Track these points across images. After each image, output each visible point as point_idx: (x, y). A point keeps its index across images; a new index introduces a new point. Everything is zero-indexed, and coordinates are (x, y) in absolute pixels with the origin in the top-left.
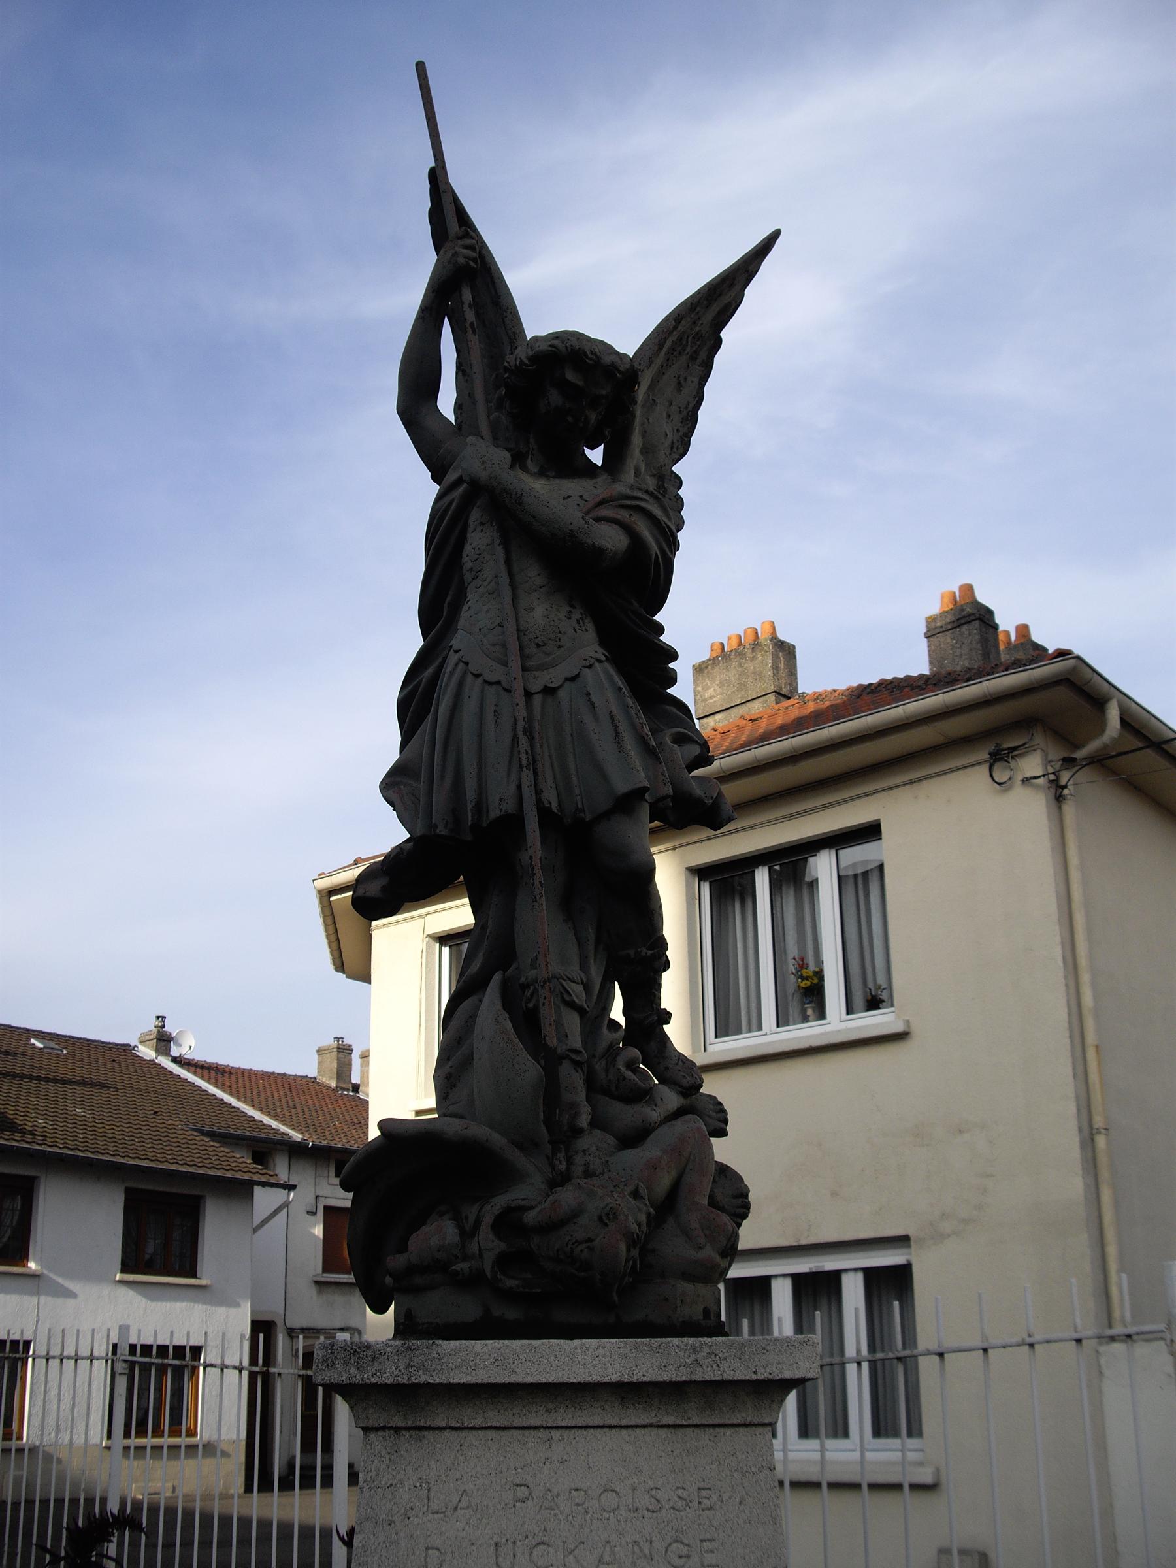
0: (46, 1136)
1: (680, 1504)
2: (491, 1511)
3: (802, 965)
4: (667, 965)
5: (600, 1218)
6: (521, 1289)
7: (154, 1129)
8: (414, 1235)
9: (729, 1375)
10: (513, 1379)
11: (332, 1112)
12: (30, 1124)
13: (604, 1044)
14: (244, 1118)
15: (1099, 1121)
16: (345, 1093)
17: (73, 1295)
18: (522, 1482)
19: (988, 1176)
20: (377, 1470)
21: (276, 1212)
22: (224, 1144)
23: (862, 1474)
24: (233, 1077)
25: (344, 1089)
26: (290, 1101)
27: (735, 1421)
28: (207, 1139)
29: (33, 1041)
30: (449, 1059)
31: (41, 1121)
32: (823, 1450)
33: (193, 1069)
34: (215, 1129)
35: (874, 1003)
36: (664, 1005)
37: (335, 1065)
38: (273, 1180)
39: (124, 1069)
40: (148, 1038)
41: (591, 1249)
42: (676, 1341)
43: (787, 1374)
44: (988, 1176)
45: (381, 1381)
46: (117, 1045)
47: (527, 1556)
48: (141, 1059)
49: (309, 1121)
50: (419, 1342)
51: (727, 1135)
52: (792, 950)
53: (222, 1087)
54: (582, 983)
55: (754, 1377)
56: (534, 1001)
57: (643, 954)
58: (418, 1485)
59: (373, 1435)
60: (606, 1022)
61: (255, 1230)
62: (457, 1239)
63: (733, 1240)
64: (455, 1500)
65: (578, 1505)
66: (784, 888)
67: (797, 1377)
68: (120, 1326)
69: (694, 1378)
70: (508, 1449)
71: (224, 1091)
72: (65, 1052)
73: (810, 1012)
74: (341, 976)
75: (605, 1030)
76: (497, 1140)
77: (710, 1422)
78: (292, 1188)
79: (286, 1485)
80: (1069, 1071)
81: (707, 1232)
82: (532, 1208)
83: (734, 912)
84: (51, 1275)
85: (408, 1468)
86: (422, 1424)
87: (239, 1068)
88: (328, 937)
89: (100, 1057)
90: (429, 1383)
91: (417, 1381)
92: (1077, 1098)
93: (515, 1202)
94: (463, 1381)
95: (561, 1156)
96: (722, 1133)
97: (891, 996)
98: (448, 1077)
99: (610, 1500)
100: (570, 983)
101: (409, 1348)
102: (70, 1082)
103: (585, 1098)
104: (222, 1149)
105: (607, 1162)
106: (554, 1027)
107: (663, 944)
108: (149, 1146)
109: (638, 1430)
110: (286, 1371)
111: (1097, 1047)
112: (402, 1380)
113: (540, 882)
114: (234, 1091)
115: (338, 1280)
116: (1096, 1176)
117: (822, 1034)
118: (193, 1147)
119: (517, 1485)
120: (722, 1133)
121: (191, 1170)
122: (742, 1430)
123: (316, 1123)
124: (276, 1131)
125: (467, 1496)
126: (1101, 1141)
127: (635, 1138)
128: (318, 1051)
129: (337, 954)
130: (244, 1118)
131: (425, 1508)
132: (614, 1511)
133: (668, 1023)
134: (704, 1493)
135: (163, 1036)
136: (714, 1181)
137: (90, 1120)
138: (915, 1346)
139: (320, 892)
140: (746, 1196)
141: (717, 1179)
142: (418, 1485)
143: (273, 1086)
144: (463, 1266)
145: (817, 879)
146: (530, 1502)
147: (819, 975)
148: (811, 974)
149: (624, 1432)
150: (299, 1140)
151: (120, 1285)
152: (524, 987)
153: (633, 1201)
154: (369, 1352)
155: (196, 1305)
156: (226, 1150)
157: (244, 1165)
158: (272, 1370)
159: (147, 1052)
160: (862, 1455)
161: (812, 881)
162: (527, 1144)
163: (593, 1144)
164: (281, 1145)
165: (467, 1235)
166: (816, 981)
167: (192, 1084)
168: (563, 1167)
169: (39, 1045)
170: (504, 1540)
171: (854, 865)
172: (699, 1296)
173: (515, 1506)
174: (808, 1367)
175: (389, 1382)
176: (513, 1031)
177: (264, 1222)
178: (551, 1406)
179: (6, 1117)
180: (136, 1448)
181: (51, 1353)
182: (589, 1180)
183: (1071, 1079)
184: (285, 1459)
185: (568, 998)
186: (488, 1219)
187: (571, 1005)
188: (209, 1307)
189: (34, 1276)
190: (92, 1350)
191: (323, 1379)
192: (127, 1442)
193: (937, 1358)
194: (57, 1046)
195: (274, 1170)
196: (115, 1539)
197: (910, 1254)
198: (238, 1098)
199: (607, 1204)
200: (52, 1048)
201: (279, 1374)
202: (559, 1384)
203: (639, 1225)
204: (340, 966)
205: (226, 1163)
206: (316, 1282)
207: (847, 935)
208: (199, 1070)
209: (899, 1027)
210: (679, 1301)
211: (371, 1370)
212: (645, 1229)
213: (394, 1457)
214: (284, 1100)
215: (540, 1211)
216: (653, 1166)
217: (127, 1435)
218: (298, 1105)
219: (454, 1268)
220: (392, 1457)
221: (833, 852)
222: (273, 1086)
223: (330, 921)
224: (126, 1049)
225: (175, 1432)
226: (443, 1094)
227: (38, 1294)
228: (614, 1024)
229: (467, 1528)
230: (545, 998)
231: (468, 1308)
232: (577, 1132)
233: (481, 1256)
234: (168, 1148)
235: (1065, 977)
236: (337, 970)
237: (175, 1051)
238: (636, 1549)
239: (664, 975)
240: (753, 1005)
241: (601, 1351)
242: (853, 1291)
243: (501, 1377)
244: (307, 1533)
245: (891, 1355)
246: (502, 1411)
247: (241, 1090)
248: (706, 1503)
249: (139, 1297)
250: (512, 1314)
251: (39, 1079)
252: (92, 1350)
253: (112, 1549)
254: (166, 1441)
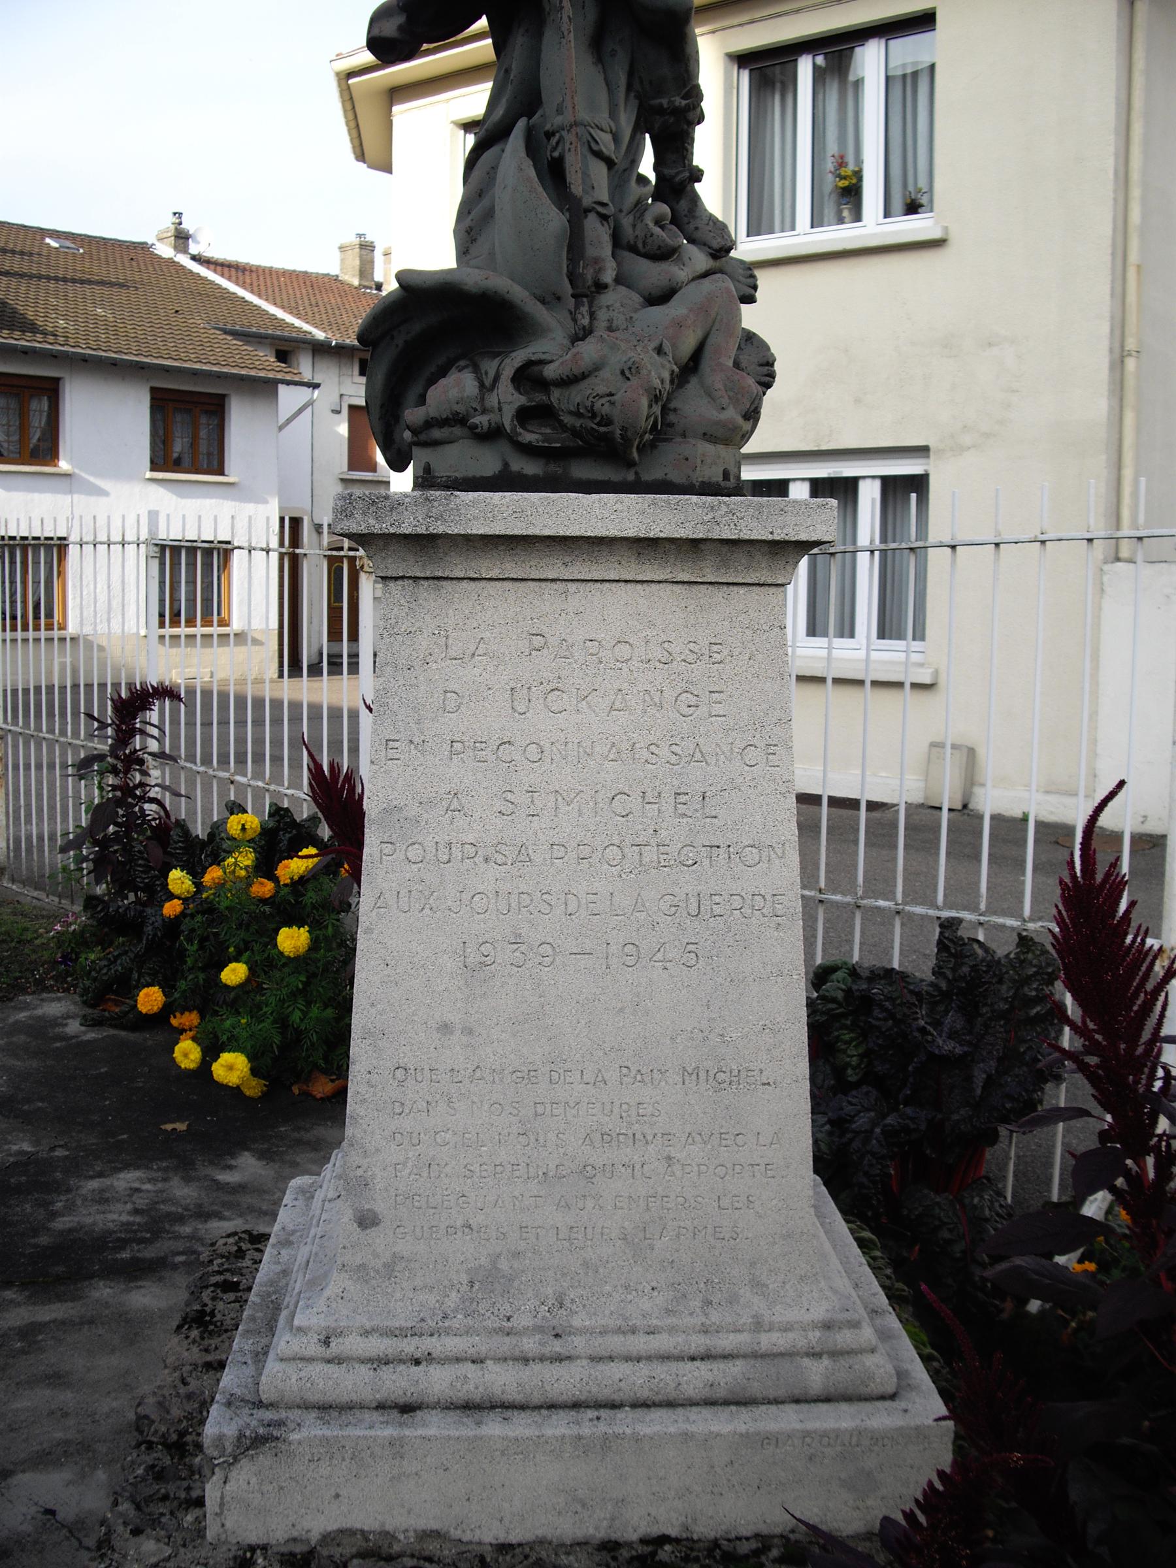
0: (67, 337)
1: (691, 658)
2: (507, 659)
3: (842, 163)
4: (701, 119)
5: (623, 373)
6: (540, 444)
7: (176, 328)
8: (433, 387)
9: (745, 535)
10: (530, 532)
11: (355, 310)
12: (51, 325)
13: (631, 200)
14: (267, 317)
15: (1131, 344)
16: (368, 291)
17: (103, 493)
18: (538, 632)
19: (1013, 391)
20: (397, 618)
21: (300, 411)
22: (247, 343)
23: (867, 670)
24: (254, 276)
25: (366, 287)
26: (312, 299)
27: (750, 581)
28: (229, 338)
29: (48, 240)
30: (469, 213)
31: (62, 322)
32: (830, 648)
33: (212, 267)
34: (237, 328)
35: (912, 208)
36: (698, 161)
37: (357, 262)
38: (296, 379)
39: (143, 267)
40: (165, 235)
41: (612, 403)
42: (694, 498)
43: (803, 537)
44: (1013, 391)
45: (399, 531)
46: (134, 243)
47: (541, 701)
48: (160, 257)
49: (332, 320)
50: (437, 493)
51: (755, 302)
52: (832, 148)
53: (243, 286)
54: (611, 132)
55: (770, 537)
56: (559, 149)
57: (677, 104)
58: (437, 632)
59: (392, 584)
60: (635, 178)
61: (281, 428)
62: (477, 391)
63: (756, 402)
64: (472, 648)
65: (592, 654)
66: (827, 80)
67: (813, 539)
68: (149, 512)
69: (710, 536)
70: (524, 600)
71: (245, 289)
72: (81, 251)
73: (846, 213)
74: (362, 166)
75: (633, 182)
76: (518, 294)
77: (725, 580)
78: (316, 386)
79: (315, 670)
80: (1107, 289)
81: (731, 394)
82: (551, 362)
83: (773, 103)
84: (83, 475)
85: (426, 617)
86: (440, 574)
87: (260, 266)
88: (347, 124)
89: (118, 256)
90: (447, 534)
91: (435, 531)
92: (1112, 318)
93: (536, 355)
94: (481, 532)
95: (584, 309)
96: (750, 299)
97: (931, 201)
98: (469, 231)
99: (623, 651)
100: (599, 131)
101: (427, 499)
102: (90, 282)
103: (610, 253)
104: (245, 347)
105: (631, 318)
106: (580, 175)
107: (695, 95)
108: (172, 344)
109: (653, 585)
110: (312, 552)
111: (1139, 266)
112: (421, 530)
113: (569, 17)
114: (256, 289)
115: (363, 478)
116: (1121, 399)
117: (856, 237)
118: (216, 345)
119: (533, 635)
120: (750, 299)
121: (215, 369)
122: (755, 589)
123: (340, 321)
124: (299, 330)
125: (484, 643)
126: (1131, 364)
127: (662, 297)
128: (340, 248)
129: (357, 142)
130: (267, 317)
131: (444, 655)
132: (627, 660)
133: (699, 180)
134: (715, 648)
135: (180, 233)
136: (739, 348)
137: (112, 320)
138: (926, 539)
139: (338, 74)
140: (772, 365)
141: (743, 346)
142: (437, 632)
143: (296, 286)
144: (481, 420)
145: (863, 79)
146: (545, 651)
147: (858, 175)
148: (849, 173)
149: (639, 586)
150: (322, 338)
151: (151, 483)
152: (549, 135)
153: (656, 356)
154: (388, 503)
155: (225, 502)
156: (250, 348)
157: (267, 363)
158: (298, 551)
159: (165, 251)
160: (868, 654)
161: (858, 80)
162: (550, 299)
163: (616, 301)
164: (304, 343)
165: (485, 388)
166: (854, 181)
167: (212, 283)
168: (586, 321)
169: (54, 244)
170: (519, 685)
171: (904, 66)
172: (719, 457)
173: (530, 654)
174: (825, 529)
175: (407, 532)
176: (536, 179)
177: (289, 421)
178: (567, 559)
179: (26, 318)
180: (171, 637)
181: (84, 540)
182: (612, 334)
183: (1108, 297)
184: (315, 649)
185: (595, 147)
186: (508, 372)
187: (598, 155)
188: (237, 503)
189: (67, 475)
190: (123, 536)
191: (342, 529)
192: (162, 631)
193: (949, 550)
194: (73, 246)
195: (298, 368)
196: (156, 708)
197: (928, 464)
198: (260, 296)
199: (630, 358)
200: (68, 248)
201: (305, 555)
202: (576, 537)
203: (662, 382)
204: (361, 156)
205: (250, 361)
206: (342, 480)
207: (891, 134)
208: (219, 268)
209: (936, 234)
210: (699, 461)
211: (389, 520)
212: (667, 386)
213: (413, 605)
214: (306, 298)
215: (562, 363)
216: (679, 324)
217: (162, 625)
218: (320, 303)
219: (472, 421)
220: (411, 606)
221: (883, 41)
222: (296, 286)
223: (349, 107)
224: (143, 247)
225: (207, 622)
226: (463, 252)
227: (71, 492)
228: (643, 180)
229: (484, 674)
230: (571, 144)
231: (487, 462)
232: (601, 287)
233: (500, 409)
234: (191, 347)
235: (1115, 191)
236: (358, 159)
237: (194, 249)
238: (647, 698)
239: (698, 128)
240: (788, 204)
241: (618, 506)
242: (869, 495)
243: (519, 530)
244: (335, 714)
245: (904, 545)
246: (519, 563)
247: (263, 288)
248: (717, 657)
249: (170, 494)
250: (531, 468)
251: (56, 279)
252: (123, 536)
253: (153, 716)
254: (199, 630)
